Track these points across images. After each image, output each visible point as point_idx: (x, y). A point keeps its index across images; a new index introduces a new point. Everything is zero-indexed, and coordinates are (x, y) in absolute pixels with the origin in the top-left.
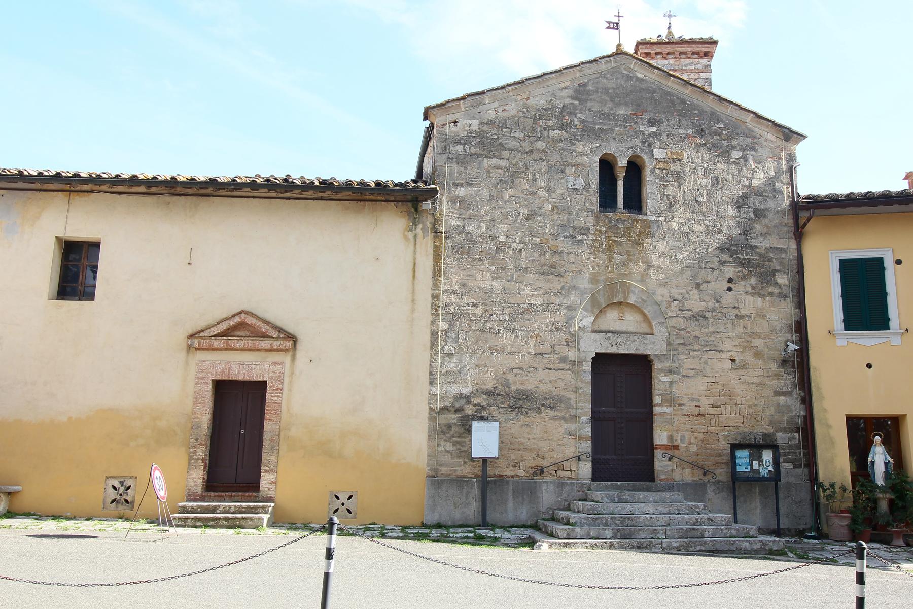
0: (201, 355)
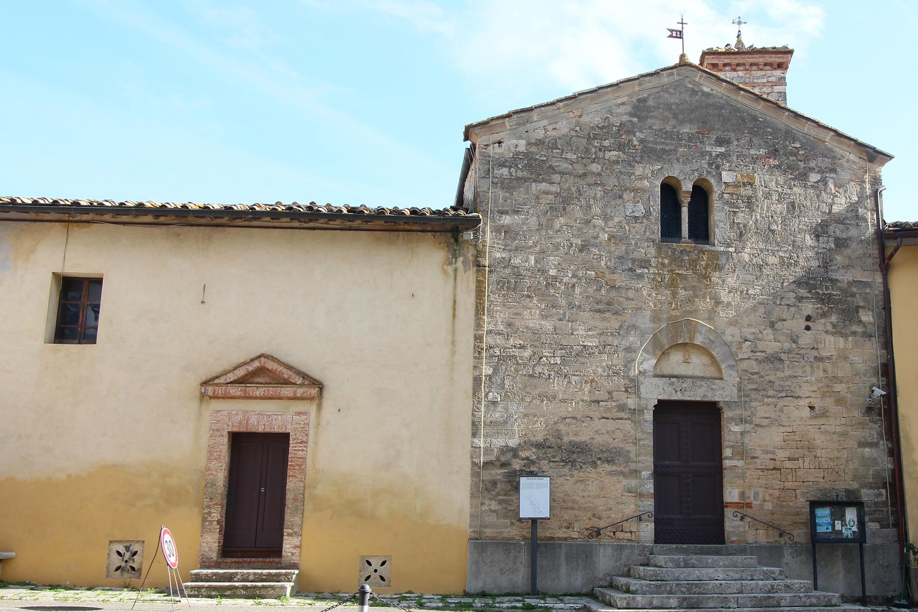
0: (216, 405)
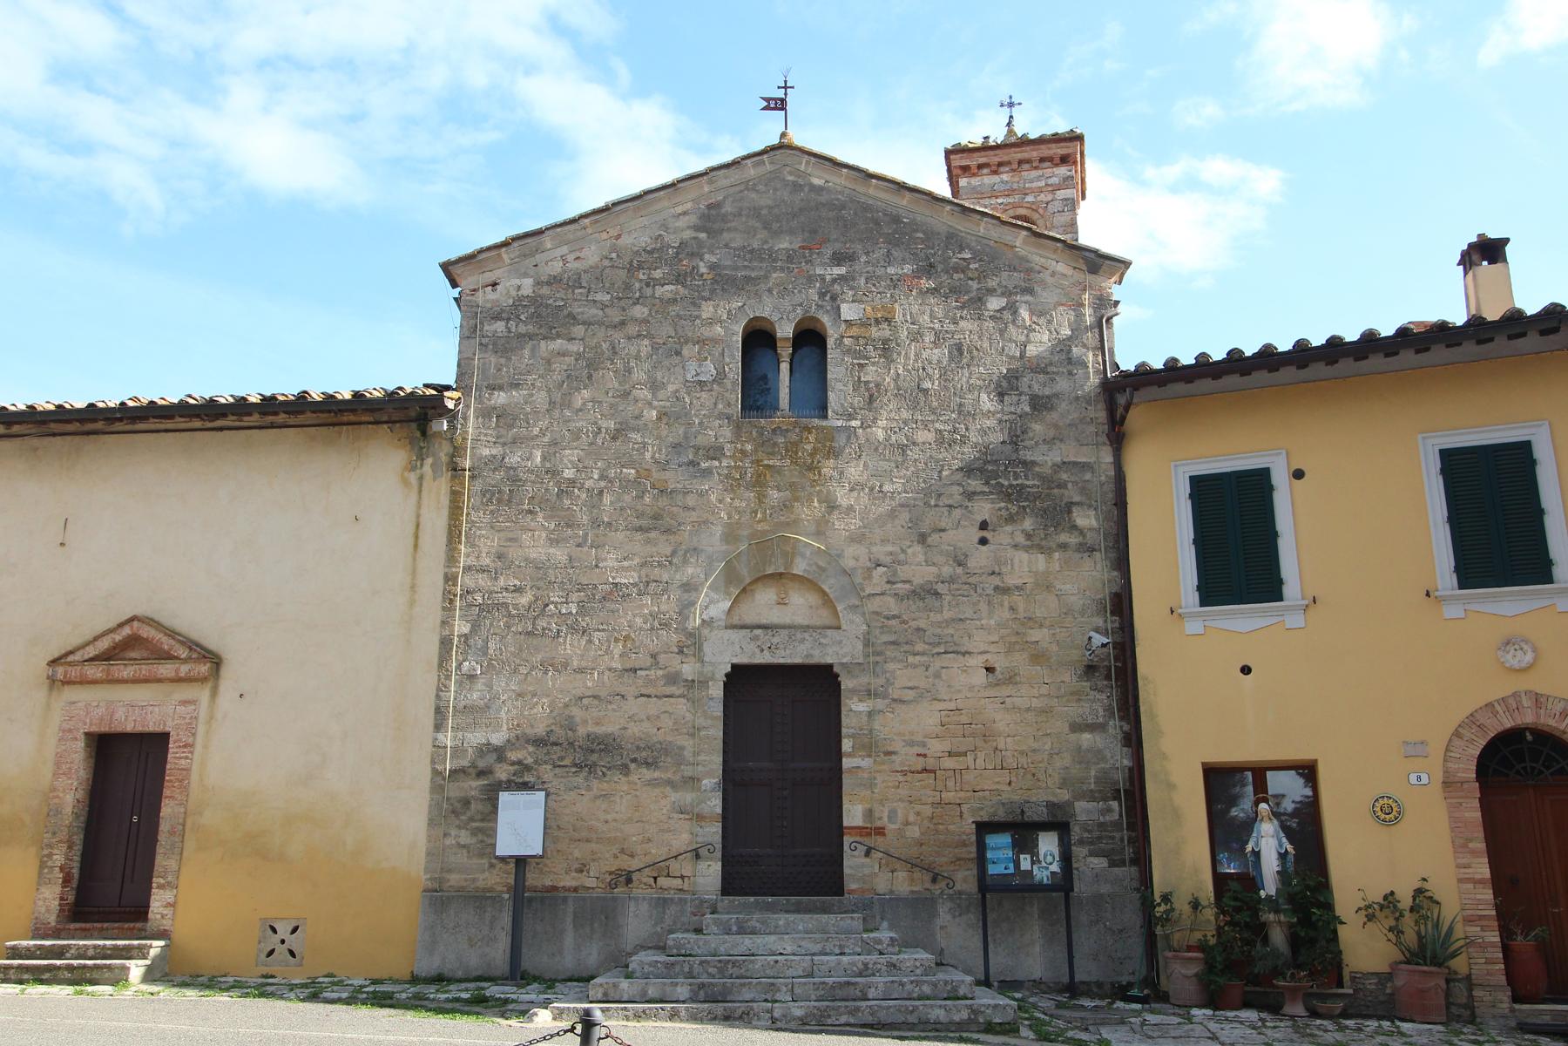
0: (71, 694)
